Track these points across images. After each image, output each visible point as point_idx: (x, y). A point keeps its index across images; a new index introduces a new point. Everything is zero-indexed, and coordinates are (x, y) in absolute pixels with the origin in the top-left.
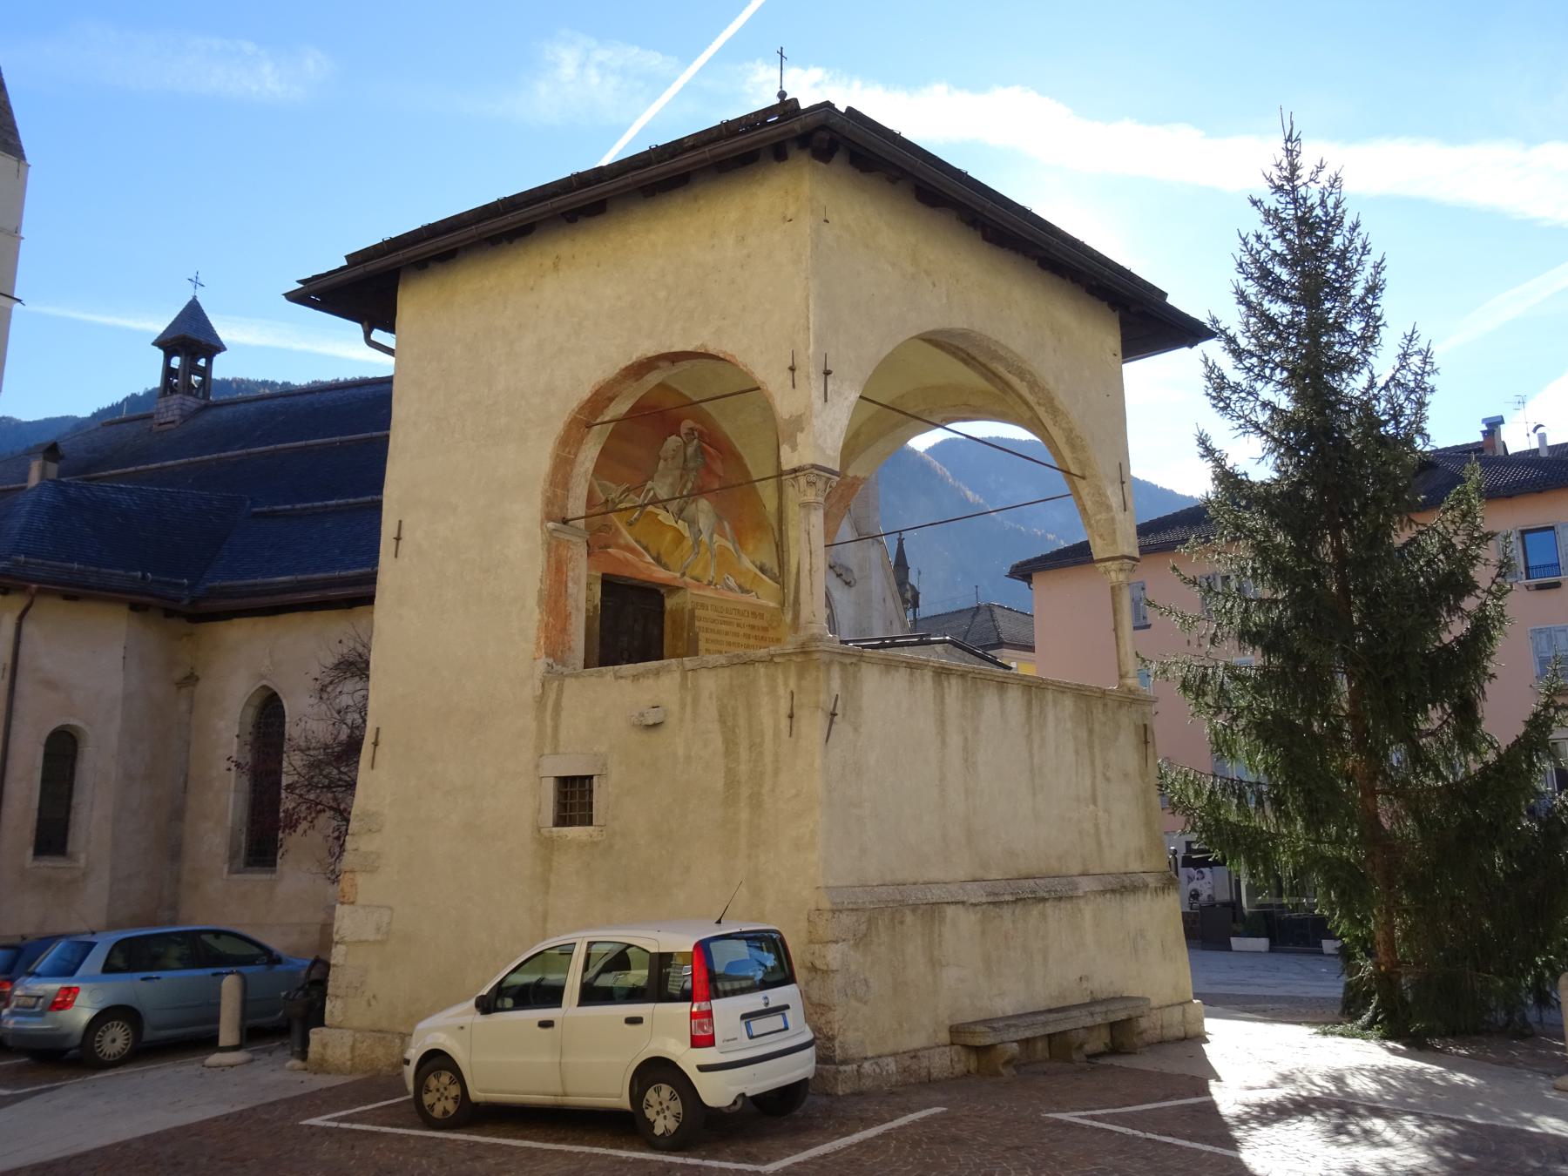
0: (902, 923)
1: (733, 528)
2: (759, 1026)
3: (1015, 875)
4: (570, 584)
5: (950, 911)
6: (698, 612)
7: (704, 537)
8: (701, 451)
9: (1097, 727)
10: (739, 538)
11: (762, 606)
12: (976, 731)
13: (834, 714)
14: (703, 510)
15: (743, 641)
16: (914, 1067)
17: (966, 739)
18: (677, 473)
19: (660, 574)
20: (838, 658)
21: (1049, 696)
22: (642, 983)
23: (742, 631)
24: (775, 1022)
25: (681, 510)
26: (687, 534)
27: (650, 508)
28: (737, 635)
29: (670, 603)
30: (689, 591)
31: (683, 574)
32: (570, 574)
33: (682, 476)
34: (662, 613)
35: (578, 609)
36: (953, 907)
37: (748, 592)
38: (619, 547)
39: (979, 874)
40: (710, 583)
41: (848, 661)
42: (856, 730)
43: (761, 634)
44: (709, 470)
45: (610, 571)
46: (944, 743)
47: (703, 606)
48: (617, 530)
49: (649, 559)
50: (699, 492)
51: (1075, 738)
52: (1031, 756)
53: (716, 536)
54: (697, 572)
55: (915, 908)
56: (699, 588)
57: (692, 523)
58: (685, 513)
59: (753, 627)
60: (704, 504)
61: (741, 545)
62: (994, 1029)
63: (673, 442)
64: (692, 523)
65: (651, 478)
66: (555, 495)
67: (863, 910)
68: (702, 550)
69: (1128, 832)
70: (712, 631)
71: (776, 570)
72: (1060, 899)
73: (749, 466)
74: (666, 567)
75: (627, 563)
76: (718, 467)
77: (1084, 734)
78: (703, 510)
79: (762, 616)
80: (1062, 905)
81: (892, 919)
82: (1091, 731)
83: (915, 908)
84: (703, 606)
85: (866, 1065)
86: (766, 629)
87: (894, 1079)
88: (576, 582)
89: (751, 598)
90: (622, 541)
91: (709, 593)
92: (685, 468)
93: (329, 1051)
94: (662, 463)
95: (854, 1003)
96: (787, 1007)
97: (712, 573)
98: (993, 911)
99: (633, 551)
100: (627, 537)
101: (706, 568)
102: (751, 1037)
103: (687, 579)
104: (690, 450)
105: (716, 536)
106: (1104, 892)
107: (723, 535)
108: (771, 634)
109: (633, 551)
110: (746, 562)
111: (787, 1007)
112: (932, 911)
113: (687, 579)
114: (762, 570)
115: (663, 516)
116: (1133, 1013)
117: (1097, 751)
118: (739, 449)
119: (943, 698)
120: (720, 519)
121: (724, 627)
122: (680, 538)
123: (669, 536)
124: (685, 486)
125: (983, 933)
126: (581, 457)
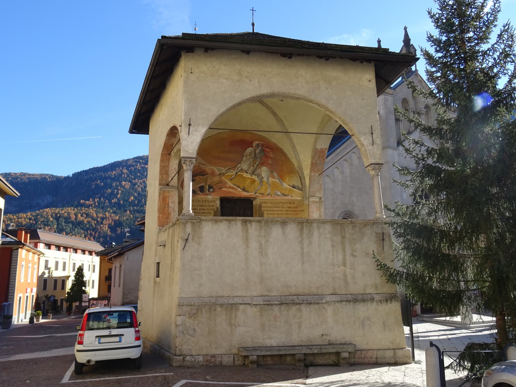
0: (215, 310)
1: (278, 174)
2: (103, 340)
3: (288, 294)
4: (170, 204)
5: (241, 307)
6: (262, 205)
7: (265, 179)
8: (262, 150)
9: (347, 235)
10: (281, 177)
11: (294, 200)
12: (267, 241)
13: (187, 240)
14: (264, 171)
15: (284, 212)
16: (212, 360)
17: (261, 245)
18: (252, 160)
19: (245, 194)
20: (189, 221)
21: (315, 225)
22: (490, 341)
23: (284, 209)
24: (117, 339)
25: (254, 172)
26: (257, 179)
27: (239, 173)
28: (282, 211)
29: (254, 203)
30: (258, 198)
31: (256, 193)
32: (170, 201)
33: (253, 161)
34: (252, 207)
35: (174, 211)
36: (243, 306)
37: (287, 195)
38: (226, 187)
39: (266, 293)
40: (268, 195)
41: (195, 221)
42: (199, 244)
43: (294, 209)
44: (267, 157)
45: (223, 196)
46: (247, 246)
47: (265, 202)
48: (225, 182)
49: (240, 190)
50: (262, 164)
51: (332, 241)
52: (302, 249)
53: (270, 179)
54: (262, 191)
55: (221, 305)
56: (263, 197)
57: (258, 175)
58: (255, 173)
59: (290, 207)
60: (264, 168)
61: (282, 179)
62: (247, 350)
63: (249, 150)
64: (258, 175)
65: (240, 163)
66: (162, 177)
67: (195, 306)
68: (264, 184)
69: (365, 277)
70: (270, 210)
71: (301, 186)
72: (311, 304)
73: (286, 152)
74: (247, 191)
75: (230, 192)
76: (271, 155)
77: (338, 239)
78: (264, 171)
79: (294, 203)
80: (312, 306)
81: (210, 309)
82: (343, 237)
83: (221, 305)
84: (265, 202)
85: (188, 358)
86: (297, 207)
87: (201, 364)
88: (173, 203)
89: (289, 198)
90: (228, 186)
91: (268, 198)
92: (255, 157)
93: (378, 360)
94: (244, 158)
95: (187, 336)
96: (123, 335)
97: (269, 191)
98: (267, 308)
99: (233, 188)
100: (230, 184)
101: (266, 190)
102: (99, 343)
103: (257, 194)
104: (257, 151)
105: (270, 179)
106: (341, 301)
107: (273, 177)
108: (299, 209)
109: (233, 188)
110: (286, 185)
111: (123, 335)
112: (231, 307)
113: (257, 194)
114: (294, 187)
115: (245, 175)
116: (339, 350)
117: (347, 246)
118: (280, 146)
119: (247, 230)
120: (272, 172)
121: (276, 209)
122: (254, 181)
123: (248, 181)
124: (255, 163)
125: (261, 315)
126: (171, 164)
